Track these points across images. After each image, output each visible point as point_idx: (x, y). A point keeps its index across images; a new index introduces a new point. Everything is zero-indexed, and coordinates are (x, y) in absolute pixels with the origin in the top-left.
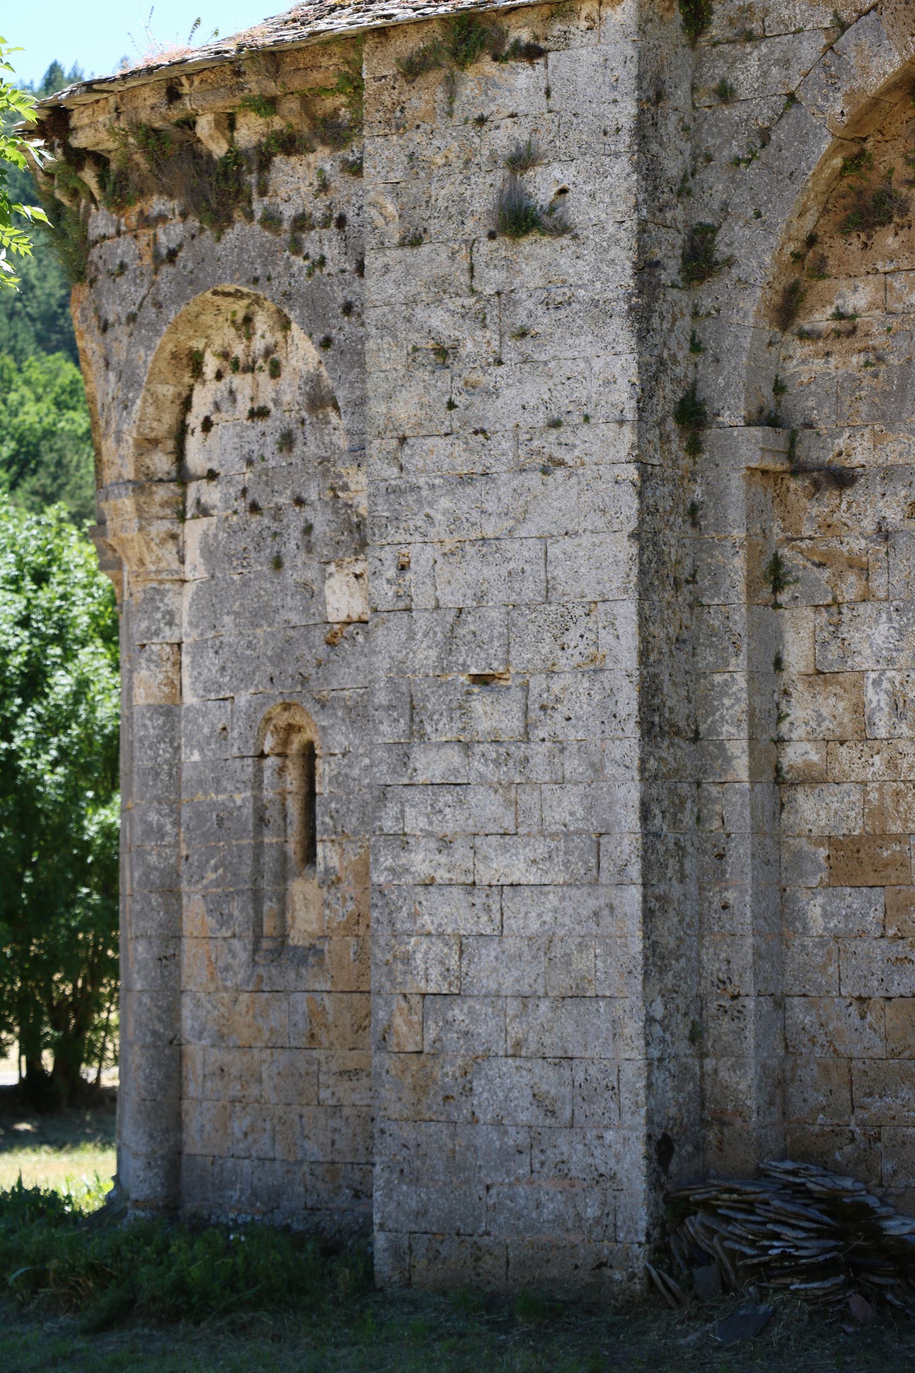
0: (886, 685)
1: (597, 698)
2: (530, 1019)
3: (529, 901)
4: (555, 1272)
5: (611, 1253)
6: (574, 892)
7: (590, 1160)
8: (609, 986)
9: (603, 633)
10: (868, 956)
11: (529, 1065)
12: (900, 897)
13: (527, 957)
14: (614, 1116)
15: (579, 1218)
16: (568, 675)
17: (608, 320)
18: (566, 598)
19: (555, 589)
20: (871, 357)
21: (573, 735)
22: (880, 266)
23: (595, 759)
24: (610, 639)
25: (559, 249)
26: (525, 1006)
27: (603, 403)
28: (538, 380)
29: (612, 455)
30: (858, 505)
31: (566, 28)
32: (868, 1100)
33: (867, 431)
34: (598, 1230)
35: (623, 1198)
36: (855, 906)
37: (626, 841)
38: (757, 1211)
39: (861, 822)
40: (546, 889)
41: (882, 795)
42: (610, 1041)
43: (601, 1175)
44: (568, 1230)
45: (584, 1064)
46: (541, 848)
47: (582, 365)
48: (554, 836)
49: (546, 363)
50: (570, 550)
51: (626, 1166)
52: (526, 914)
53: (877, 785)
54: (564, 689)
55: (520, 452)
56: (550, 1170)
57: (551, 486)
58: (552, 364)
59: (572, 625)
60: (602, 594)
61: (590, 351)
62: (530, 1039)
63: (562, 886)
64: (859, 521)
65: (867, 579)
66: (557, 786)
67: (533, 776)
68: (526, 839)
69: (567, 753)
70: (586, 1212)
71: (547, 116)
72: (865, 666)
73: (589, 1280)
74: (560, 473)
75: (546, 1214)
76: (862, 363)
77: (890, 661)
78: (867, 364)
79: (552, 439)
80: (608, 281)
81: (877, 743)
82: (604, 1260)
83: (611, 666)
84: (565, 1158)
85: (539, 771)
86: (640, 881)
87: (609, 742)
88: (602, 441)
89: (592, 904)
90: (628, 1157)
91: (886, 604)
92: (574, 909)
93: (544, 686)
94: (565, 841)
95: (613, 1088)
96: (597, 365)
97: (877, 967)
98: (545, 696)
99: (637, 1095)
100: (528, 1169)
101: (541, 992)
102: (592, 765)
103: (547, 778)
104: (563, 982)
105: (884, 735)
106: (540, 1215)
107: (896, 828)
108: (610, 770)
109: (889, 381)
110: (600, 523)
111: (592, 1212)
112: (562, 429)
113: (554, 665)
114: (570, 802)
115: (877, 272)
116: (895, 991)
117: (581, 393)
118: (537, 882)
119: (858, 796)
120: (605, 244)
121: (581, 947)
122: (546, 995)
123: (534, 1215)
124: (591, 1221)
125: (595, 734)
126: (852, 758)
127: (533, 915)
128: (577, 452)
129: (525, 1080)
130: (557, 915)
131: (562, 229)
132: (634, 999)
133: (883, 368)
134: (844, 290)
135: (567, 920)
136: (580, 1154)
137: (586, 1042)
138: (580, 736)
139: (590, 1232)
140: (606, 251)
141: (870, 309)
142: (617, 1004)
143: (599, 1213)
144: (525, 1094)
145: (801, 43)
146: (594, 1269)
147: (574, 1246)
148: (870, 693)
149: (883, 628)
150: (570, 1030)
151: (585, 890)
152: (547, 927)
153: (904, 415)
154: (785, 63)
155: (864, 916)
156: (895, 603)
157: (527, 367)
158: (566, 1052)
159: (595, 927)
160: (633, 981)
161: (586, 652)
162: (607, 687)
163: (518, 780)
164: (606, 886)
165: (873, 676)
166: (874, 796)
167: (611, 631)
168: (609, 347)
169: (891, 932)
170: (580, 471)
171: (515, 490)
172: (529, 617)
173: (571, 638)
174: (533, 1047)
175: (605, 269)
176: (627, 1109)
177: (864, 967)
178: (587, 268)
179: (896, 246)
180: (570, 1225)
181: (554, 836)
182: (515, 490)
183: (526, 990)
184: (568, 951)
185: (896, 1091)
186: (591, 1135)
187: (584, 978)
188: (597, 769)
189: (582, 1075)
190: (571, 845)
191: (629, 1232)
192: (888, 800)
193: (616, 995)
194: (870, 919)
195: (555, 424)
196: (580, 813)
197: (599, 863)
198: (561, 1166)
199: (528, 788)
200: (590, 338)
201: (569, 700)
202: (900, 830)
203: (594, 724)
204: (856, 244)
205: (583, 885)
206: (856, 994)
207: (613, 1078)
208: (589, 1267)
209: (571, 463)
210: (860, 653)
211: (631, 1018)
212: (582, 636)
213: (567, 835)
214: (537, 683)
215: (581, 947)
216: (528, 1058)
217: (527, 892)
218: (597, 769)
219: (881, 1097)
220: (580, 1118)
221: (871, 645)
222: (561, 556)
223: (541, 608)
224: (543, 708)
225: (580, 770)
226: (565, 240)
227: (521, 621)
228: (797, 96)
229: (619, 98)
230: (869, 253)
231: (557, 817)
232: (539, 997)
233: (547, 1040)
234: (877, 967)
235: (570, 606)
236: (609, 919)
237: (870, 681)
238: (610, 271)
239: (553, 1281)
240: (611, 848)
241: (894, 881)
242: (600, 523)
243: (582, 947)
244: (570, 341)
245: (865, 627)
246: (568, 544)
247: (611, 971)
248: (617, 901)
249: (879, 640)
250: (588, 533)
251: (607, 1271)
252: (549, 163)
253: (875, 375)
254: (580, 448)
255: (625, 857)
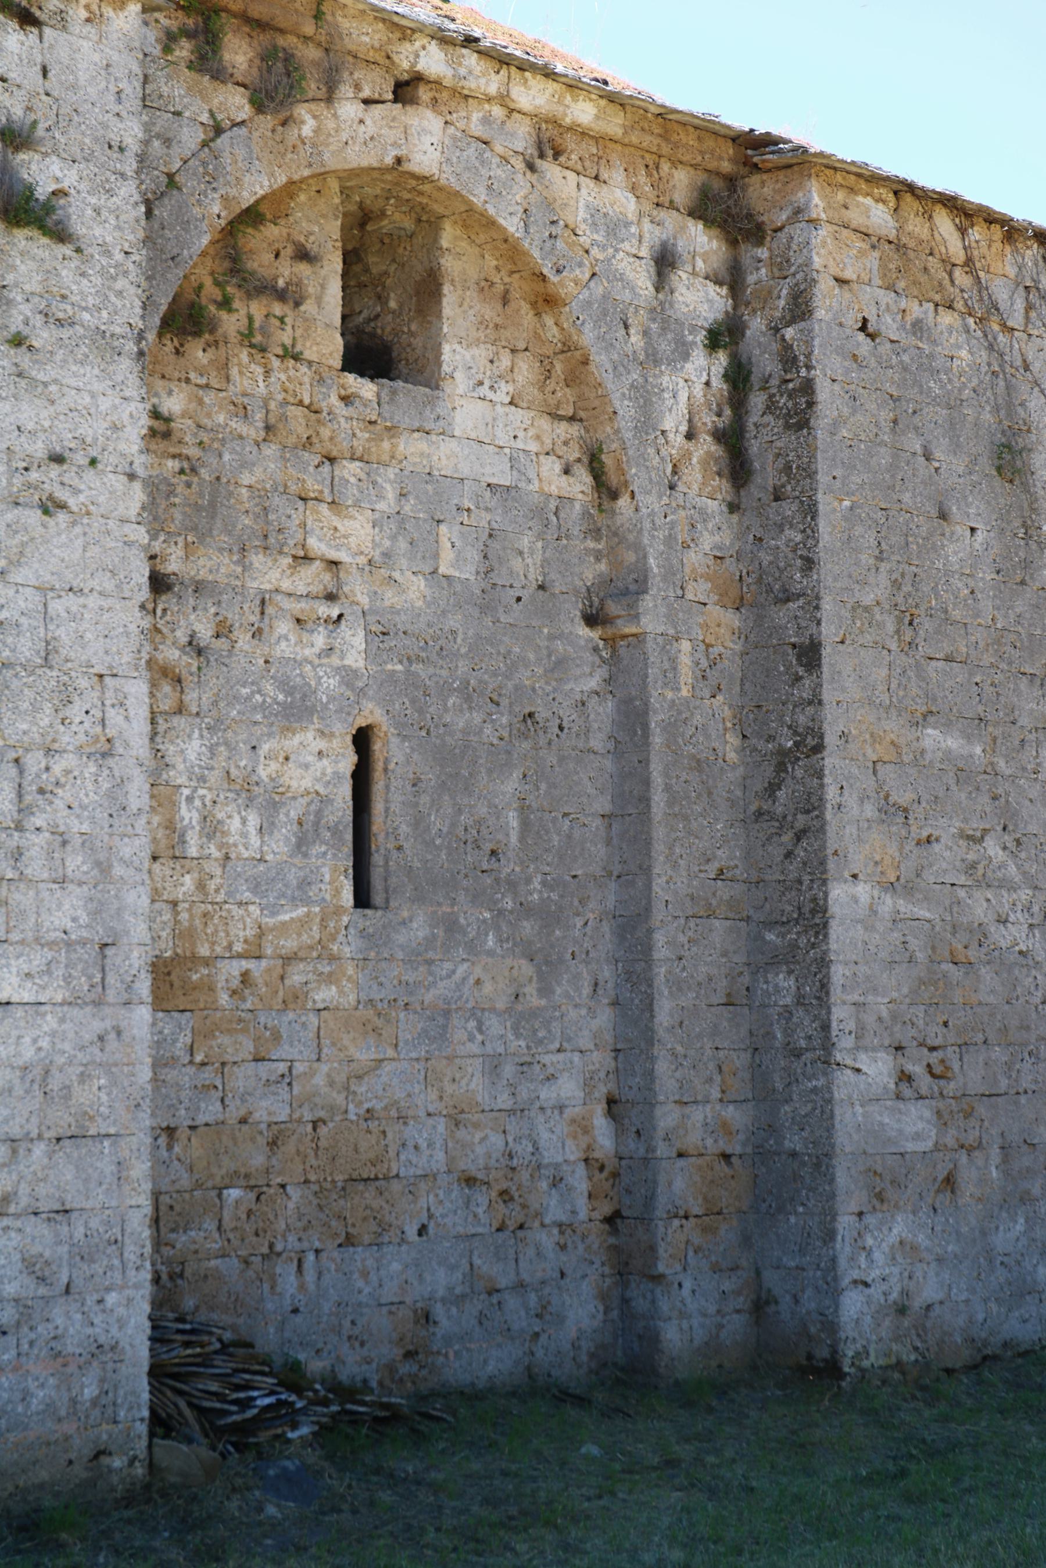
0: (197, 803)
1: (106, 785)
2: (21, 1167)
3: (22, 1024)
4: (44, 1475)
5: (110, 1436)
6: (75, 1012)
7: (89, 1331)
8: (115, 1122)
9: (111, 713)
10: (177, 1084)
11: (18, 1224)
12: (208, 1022)
13: (19, 1091)
14: (117, 1275)
15: (74, 1401)
16: (71, 756)
17: (116, 358)
18: (69, 665)
19: (57, 652)
20: (186, 465)
21: (76, 826)
22: (192, 375)
23: (102, 856)
24: (120, 719)
25: (60, 257)
26: (14, 1151)
27: (111, 449)
28: (36, 400)
29: (121, 511)
30: (172, 615)
31: (62, 7)
32: (173, 1236)
33: (180, 540)
34: (96, 1413)
35: (124, 1370)
36: (166, 1031)
37: (136, 954)
38: (216, 1363)
39: (171, 944)
40: (43, 1008)
41: (191, 915)
42: (115, 1187)
43: (100, 1347)
44: (60, 1420)
45: (84, 1217)
46: (38, 959)
47: (88, 399)
48: (51, 944)
49: (45, 384)
50: (74, 609)
51: (130, 1332)
52: (19, 1037)
53: (186, 905)
54: (67, 772)
55: (15, 481)
56: (41, 1350)
57: (52, 530)
58: (53, 388)
59: (77, 698)
60: (111, 667)
61: (97, 387)
62: (21, 1192)
63: (62, 1004)
64: (173, 631)
65: (182, 692)
66: (56, 886)
67: (28, 871)
68: (19, 948)
69: (69, 848)
70: (82, 1395)
71: (44, 98)
72: (179, 781)
73: (84, 1475)
74: (62, 517)
75: (35, 1404)
76: (177, 470)
77: (202, 779)
78: (182, 471)
79: (53, 474)
80: (116, 313)
81: (188, 861)
82: (102, 1448)
83: (121, 751)
84: (60, 1332)
85: (36, 867)
86: (150, 1000)
87: (117, 838)
88: (110, 493)
89: (98, 1026)
90: (133, 1321)
91: (198, 720)
92: (76, 1033)
93: (43, 765)
94: (67, 952)
95: (116, 1242)
96: (105, 404)
97: (185, 1095)
98: (44, 776)
99: (143, 1247)
100: (13, 1352)
101: (34, 1134)
102: (98, 864)
103: (45, 876)
104: (62, 1120)
105: (195, 854)
106: (28, 1406)
107: (204, 951)
108: (118, 870)
109: (201, 495)
110: (109, 585)
111: (90, 1392)
112: (65, 467)
113: (54, 741)
114: (72, 906)
115: (188, 381)
116: (201, 1119)
117: (86, 430)
118: (32, 1000)
119: (169, 916)
120: (112, 270)
121: (83, 1078)
122: (40, 1137)
123: (20, 1409)
124: (88, 1404)
125: (102, 828)
126: (164, 876)
127: (27, 1040)
128: (82, 498)
129: (14, 1243)
130: (56, 1040)
131: (60, 235)
132: (142, 1135)
133: (196, 479)
134: (160, 390)
135: (67, 1046)
136: (78, 1326)
137: (88, 1190)
138: (85, 828)
139: (87, 1417)
140: (114, 278)
141: (183, 416)
142: (122, 1143)
143: (97, 1392)
144: (14, 1260)
145: (181, 126)
146: (91, 1461)
147: (67, 1438)
148: (184, 810)
149: (196, 744)
150: (69, 1177)
151: (88, 1009)
152: (43, 1054)
153: (215, 533)
154: (167, 142)
155: (175, 1041)
156: (206, 720)
157: (23, 383)
158: (63, 1204)
159: (100, 1054)
160: (141, 1115)
161: (92, 732)
162: (117, 774)
163: (9, 876)
164: (113, 1005)
165: (186, 792)
166: (184, 916)
167: (121, 711)
168: (118, 388)
169: (199, 1058)
170: (85, 521)
171: (8, 526)
172: (25, 680)
173: (76, 712)
174: (24, 1201)
175: (113, 299)
176: (131, 1265)
177: (173, 1095)
178: (93, 290)
179: (205, 361)
180: (63, 1413)
181: (51, 944)
182: (8, 526)
183: (16, 1132)
184: (67, 1083)
185: (200, 1223)
186: (91, 1300)
187: (86, 1113)
188: (104, 868)
189: (82, 1230)
190: (74, 956)
191: (131, 1408)
192: (197, 921)
193: (122, 1132)
194: (179, 1045)
195: (58, 459)
196: (84, 919)
197: (103, 979)
198: (53, 1344)
199: (22, 886)
200: (96, 371)
201: (73, 785)
202: (208, 954)
203: (101, 815)
204: (169, 347)
205: (86, 1004)
206: (164, 1125)
207: (117, 1230)
208: (85, 1459)
209: (75, 509)
210: (174, 767)
211: (137, 1158)
212: (87, 712)
213: (69, 944)
214: (34, 762)
215: (83, 1078)
216: (17, 1216)
217: (20, 1012)
218: (104, 868)
219: (185, 1232)
220: (78, 1283)
221: (185, 761)
222: (64, 614)
223: (39, 671)
224: (41, 791)
225: (85, 868)
226: (67, 250)
227: (15, 684)
228: (177, 178)
229: (124, 114)
230: (182, 360)
231: (57, 922)
232: (32, 1140)
233: (42, 1190)
234: (185, 1095)
235: (73, 674)
236: (116, 1044)
237: (184, 797)
238: (119, 303)
239: (41, 1486)
240: (118, 961)
241: (202, 1006)
242: (109, 585)
243: (84, 1078)
244: (74, 368)
245: (179, 741)
246: (72, 602)
247: (117, 1105)
248: (126, 1023)
249: (192, 756)
250: (95, 593)
251: (105, 1460)
252: (46, 155)
253: (189, 485)
254: (85, 494)
255: (134, 972)
